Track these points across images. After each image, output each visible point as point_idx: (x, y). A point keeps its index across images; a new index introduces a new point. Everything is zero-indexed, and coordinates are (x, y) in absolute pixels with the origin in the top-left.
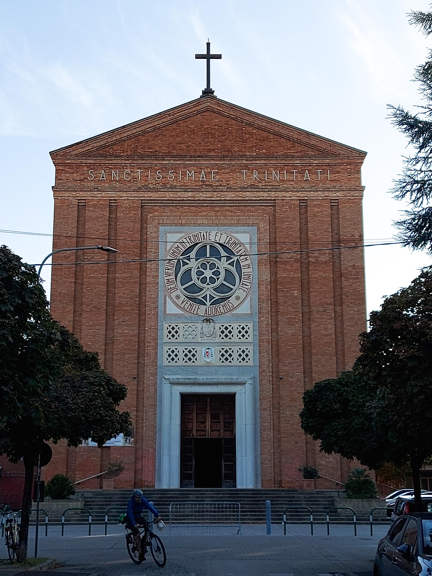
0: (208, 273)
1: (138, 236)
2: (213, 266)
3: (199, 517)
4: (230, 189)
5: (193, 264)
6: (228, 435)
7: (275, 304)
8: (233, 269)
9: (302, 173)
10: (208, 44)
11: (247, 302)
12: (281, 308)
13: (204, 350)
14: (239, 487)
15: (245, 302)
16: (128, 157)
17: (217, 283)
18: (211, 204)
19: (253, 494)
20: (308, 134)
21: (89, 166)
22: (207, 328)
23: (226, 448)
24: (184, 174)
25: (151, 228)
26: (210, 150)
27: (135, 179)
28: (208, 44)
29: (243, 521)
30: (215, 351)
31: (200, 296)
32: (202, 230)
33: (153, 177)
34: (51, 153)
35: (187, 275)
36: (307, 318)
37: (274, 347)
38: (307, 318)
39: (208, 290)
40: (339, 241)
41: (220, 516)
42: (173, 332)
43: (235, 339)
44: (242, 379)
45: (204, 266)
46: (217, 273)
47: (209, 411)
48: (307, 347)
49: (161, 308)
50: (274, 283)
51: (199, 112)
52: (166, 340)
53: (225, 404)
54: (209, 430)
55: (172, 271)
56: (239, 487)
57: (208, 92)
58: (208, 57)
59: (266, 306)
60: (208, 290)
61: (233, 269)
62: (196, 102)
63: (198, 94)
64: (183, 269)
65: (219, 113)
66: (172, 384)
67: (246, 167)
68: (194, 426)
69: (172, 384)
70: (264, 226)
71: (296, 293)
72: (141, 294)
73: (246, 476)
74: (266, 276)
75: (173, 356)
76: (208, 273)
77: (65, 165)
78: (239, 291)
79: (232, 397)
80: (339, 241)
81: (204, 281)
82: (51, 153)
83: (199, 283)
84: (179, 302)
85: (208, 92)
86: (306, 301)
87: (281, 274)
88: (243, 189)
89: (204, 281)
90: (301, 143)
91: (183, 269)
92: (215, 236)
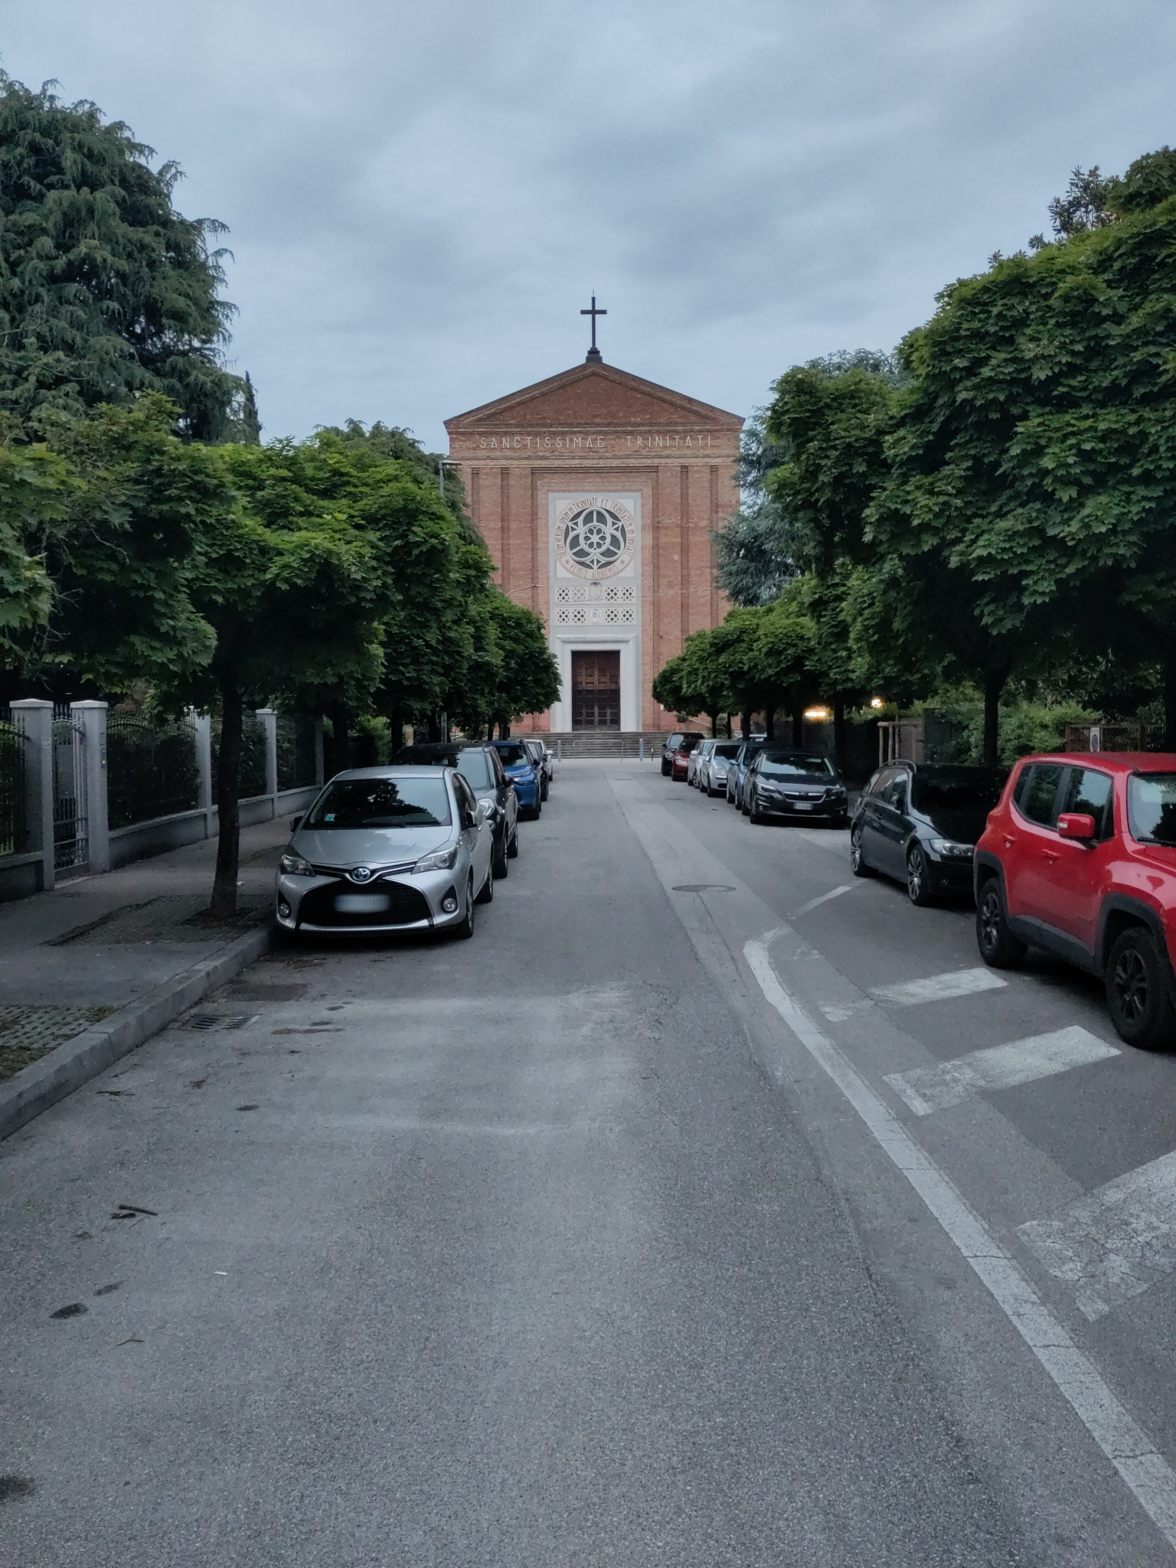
0: (595, 538)
1: (529, 503)
2: (599, 531)
3: (590, 752)
4: (615, 457)
5: (581, 530)
6: (613, 687)
7: (656, 567)
8: (618, 534)
9: (684, 439)
10: (593, 299)
11: (631, 567)
12: (663, 572)
13: (592, 611)
14: (623, 730)
15: (630, 565)
16: (517, 425)
17: (603, 548)
18: (598, 471)
19: (635, 736)
20: (690, 400)
21: (481, 434)
22: (595, 590)
23: (612, 698)
24: (571, 441)
25: (540, 495)
26: (596, 416)
27: (525, 446)
28: (593, 299)
29: (625, 756)
30: (602, 612)
31: (587, 560)
32: (589, 496)
33: (544, 444)
34: (445, 423)
35: (575, 542)
36: (685, 581)
37: (657, 609)
38: (685, 581)
39: (595, 554)
40: (717, 506)
41: (606, 751)
42: (563, 595)
43: (620, 601)
44: (626, 636)
45: (591, 531)
46: (603, 538)
47: (598, 664)
48: (684, 607)
49: (551, 573)
50: (656, 547)
51: (586, 377)
52: (634, 609)
53: (609, 660)
54: (595, 681)
55: (562, 537)
56: (623, 730)
57: (594, 353)
58: (594, 312)
59: (649, 569)
60: (595, 554)
61: (618, 534)
62: (582, 367)
63: (580, 359)
64: (572, 534)
65: (605, 378)
66: (564, 642)
67: (631, 433)
68: (583, 679)
69: (564, 642)
70: (648, 491)
71: (676, 557)
72: (534, 559)
73: (629, 722)
74: (649, 541)
75: (563, 616)
76: (595, 538)
77: (458, 433)
78: (623, 555)
79: (615, 655)
80: (717, 506)
81: (591, 545)
82: (445, 423)
83: (587, 549)
84: (568, 566)
85: (594, 353)
86: (684, 564)
87: (663, 540)
88: (628, 457)
89: (591, 545)
90: (683, 408)
91: (572, 534)
92: (601, 501)
